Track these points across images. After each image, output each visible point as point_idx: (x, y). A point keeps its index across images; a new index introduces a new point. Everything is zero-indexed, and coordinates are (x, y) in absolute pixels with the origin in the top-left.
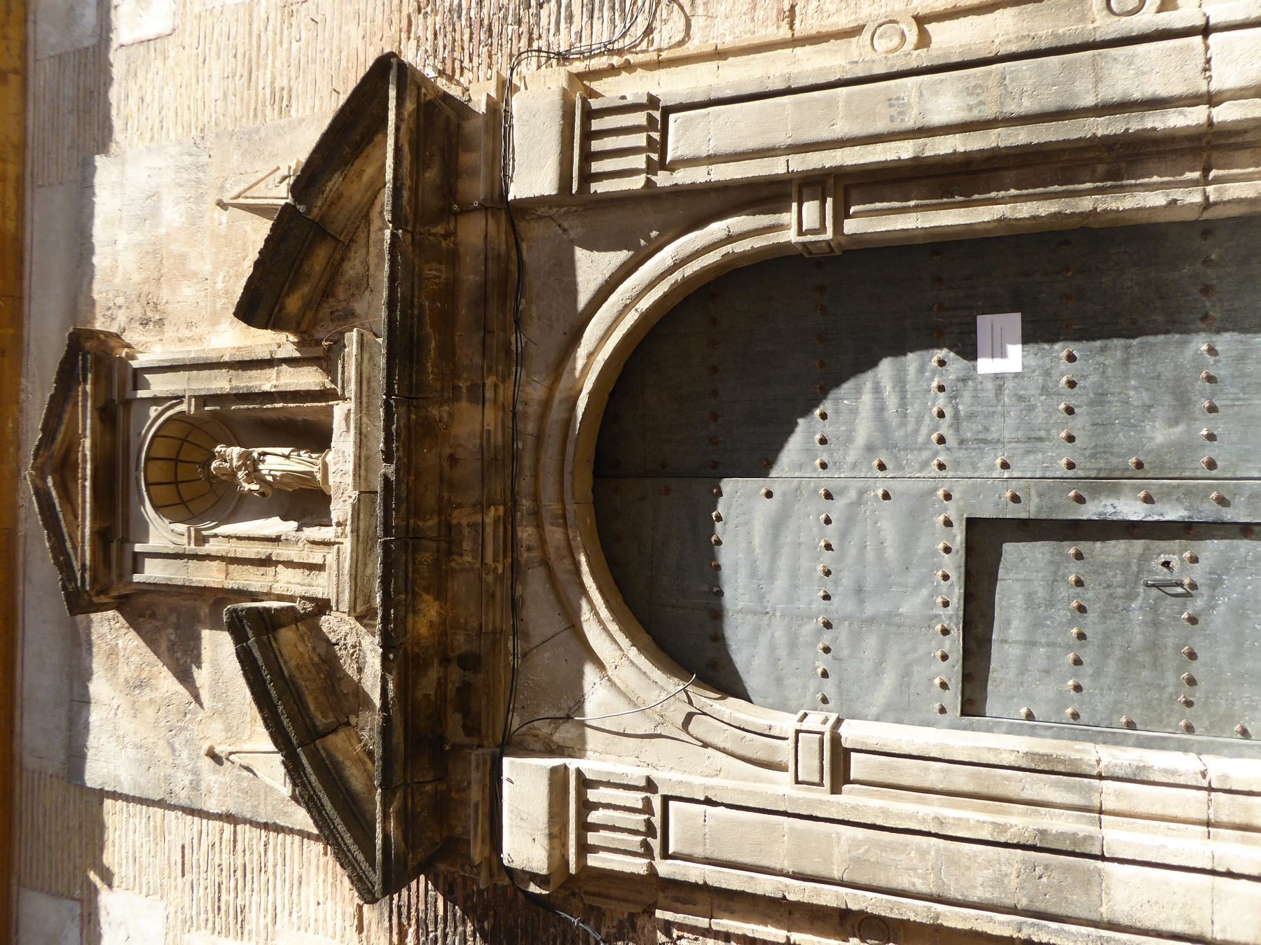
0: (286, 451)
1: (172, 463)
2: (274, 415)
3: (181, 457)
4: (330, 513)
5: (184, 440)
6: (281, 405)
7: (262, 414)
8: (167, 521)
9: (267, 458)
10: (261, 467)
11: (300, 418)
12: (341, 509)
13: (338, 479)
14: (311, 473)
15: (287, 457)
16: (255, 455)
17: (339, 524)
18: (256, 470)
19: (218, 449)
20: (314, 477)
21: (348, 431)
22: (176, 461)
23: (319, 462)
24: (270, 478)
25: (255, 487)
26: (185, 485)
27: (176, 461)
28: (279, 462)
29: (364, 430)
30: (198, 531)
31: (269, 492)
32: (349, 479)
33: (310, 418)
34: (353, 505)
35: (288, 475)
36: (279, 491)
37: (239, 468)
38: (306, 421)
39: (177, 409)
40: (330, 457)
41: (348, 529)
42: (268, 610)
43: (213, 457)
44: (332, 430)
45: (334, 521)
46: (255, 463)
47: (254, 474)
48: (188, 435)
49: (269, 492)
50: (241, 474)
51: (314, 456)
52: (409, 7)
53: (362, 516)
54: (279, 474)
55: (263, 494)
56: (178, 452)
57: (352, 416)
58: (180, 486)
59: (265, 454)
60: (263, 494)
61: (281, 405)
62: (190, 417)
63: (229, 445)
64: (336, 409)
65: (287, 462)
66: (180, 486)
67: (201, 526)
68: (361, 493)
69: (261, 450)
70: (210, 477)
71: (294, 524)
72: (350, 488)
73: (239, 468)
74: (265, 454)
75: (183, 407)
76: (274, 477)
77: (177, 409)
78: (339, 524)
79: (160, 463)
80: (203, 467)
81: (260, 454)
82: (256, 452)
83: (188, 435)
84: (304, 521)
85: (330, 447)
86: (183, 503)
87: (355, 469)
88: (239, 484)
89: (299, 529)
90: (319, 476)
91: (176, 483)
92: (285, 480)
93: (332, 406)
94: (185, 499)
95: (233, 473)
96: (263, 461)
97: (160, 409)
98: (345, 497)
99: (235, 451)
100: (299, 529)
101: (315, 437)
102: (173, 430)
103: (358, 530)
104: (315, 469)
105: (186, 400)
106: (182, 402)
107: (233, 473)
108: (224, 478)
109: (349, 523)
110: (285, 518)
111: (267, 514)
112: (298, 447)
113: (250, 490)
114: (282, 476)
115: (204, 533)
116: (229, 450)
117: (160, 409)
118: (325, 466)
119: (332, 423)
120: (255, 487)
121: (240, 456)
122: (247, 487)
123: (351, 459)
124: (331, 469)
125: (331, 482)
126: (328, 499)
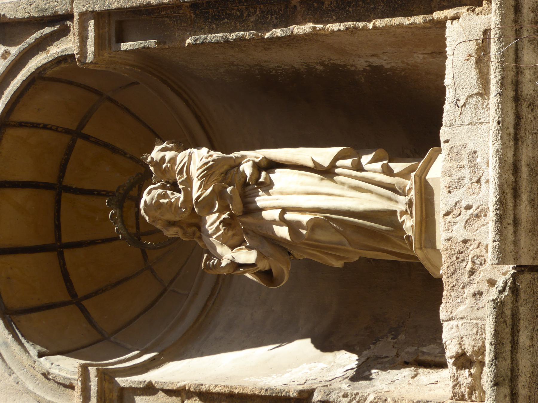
0: (324, 155)
1: (48, 196)
2: (292, 58)
3: (69, 180)
4: (439, 329)
5: (77, 134)
6: (306, 28)
7: (259, 56)
8: (33, 351)
9: (279, 177)
10: (261, 200)
11: (361, 64)
12: (466, 319)
13: (459, 232)
14: (388, 217)
15: (327, 172)
16: (247, 168)
17: (463, 361)
18: (252, 211)
19: (156, 154)
20: (399, 227)
21: (484, 93)
22: (58, 189)
23: (410, 184)
24: (283, 232)
25: (246, 256)
26: (80, 252)
27: (58, 189)
28: (306, 186)
29: (527, 89)
30: (107, 377)
31: (282, 268)
32: (487, 231)
33: (385, 61)
34: (499, 307)
35: (329, 220)
36: (312, 266)
37: (207, 205)
38: (376, 70)
39: (55, 50)
40: (437, 171)
41: (487, 376)
42: (340, 20)
43: (144, 178)
44: (442, 91)
45: (451, 350)
46: (249, 188)
47: (246, 223)
48: (82, 125)
49: (282, 268)
50: (212, 221)
51: (397, 167)
52: (535, 68)
53: (524, 339)
54: (305, 218)
55: (267, 275)
56: (58, 227)
57: (494, 48)
58: (67, 254)
59: (272, 165)
60: (267, 275)
61: (306, 28)
62: (86, 70)
63: (181, 147)
64: (452, 32)
65: (327, 186)
66: (67, 254)
67: (116, 363)
68: (520, 269)
69: (259, 154)
70: (140, 232)
71: (347, 360)
72: (490, 256)
73: (207, 205)
74: (272, 165)
75: (69, 45)
76: (294, 227)
77: (55, 50)
78: (463, 361)
79: (19, 196)
80: (120, 206)
81: (258, 167)
82: (249, 159)
83: (82, 125)
84: (375, 350)
85: (437, 143)
86: (75, 300)
87: (501, 203)
88: (213, 254)
89: (361, 374)
90: (409, 224)
91: (58, 248)
92: (322, 236)
93: (441, 25)
94: (81, 290)
95: (192, 221)
96: (268, 186)
97: (14, 50)
98: (479, 282)
99: (199, 157)
100: (361, 374)
101: (399, 116)
102: (47, 107)
103: (513, 378)
104: (400, 204)
105: (74, 25)
106: (64, 32)
107: (192, 221)
108: (171, 233)
109: (488, 357)
110: (325, 344)
111: (282, 335)
112: (355, 143)
113: (235, 265)
114: (314, 225)
115: (123, 381)
116: (182, 156)
117: (14, 50)
118: (426, 194)
119: (442, 76)
120: (246, 256)
121: (209, 172)
122: (227, 255)
123: (491, 173)
124: (442, 203)
125: (441, 243)
126: (430, 289)
